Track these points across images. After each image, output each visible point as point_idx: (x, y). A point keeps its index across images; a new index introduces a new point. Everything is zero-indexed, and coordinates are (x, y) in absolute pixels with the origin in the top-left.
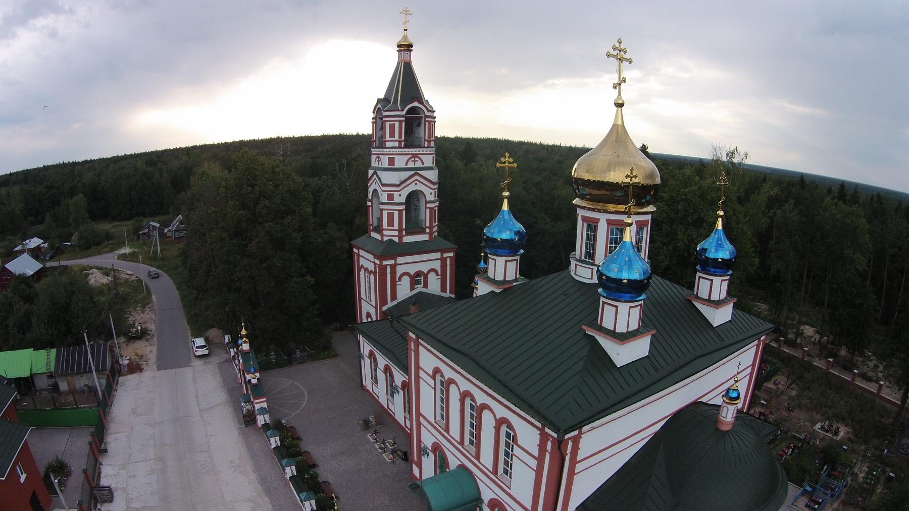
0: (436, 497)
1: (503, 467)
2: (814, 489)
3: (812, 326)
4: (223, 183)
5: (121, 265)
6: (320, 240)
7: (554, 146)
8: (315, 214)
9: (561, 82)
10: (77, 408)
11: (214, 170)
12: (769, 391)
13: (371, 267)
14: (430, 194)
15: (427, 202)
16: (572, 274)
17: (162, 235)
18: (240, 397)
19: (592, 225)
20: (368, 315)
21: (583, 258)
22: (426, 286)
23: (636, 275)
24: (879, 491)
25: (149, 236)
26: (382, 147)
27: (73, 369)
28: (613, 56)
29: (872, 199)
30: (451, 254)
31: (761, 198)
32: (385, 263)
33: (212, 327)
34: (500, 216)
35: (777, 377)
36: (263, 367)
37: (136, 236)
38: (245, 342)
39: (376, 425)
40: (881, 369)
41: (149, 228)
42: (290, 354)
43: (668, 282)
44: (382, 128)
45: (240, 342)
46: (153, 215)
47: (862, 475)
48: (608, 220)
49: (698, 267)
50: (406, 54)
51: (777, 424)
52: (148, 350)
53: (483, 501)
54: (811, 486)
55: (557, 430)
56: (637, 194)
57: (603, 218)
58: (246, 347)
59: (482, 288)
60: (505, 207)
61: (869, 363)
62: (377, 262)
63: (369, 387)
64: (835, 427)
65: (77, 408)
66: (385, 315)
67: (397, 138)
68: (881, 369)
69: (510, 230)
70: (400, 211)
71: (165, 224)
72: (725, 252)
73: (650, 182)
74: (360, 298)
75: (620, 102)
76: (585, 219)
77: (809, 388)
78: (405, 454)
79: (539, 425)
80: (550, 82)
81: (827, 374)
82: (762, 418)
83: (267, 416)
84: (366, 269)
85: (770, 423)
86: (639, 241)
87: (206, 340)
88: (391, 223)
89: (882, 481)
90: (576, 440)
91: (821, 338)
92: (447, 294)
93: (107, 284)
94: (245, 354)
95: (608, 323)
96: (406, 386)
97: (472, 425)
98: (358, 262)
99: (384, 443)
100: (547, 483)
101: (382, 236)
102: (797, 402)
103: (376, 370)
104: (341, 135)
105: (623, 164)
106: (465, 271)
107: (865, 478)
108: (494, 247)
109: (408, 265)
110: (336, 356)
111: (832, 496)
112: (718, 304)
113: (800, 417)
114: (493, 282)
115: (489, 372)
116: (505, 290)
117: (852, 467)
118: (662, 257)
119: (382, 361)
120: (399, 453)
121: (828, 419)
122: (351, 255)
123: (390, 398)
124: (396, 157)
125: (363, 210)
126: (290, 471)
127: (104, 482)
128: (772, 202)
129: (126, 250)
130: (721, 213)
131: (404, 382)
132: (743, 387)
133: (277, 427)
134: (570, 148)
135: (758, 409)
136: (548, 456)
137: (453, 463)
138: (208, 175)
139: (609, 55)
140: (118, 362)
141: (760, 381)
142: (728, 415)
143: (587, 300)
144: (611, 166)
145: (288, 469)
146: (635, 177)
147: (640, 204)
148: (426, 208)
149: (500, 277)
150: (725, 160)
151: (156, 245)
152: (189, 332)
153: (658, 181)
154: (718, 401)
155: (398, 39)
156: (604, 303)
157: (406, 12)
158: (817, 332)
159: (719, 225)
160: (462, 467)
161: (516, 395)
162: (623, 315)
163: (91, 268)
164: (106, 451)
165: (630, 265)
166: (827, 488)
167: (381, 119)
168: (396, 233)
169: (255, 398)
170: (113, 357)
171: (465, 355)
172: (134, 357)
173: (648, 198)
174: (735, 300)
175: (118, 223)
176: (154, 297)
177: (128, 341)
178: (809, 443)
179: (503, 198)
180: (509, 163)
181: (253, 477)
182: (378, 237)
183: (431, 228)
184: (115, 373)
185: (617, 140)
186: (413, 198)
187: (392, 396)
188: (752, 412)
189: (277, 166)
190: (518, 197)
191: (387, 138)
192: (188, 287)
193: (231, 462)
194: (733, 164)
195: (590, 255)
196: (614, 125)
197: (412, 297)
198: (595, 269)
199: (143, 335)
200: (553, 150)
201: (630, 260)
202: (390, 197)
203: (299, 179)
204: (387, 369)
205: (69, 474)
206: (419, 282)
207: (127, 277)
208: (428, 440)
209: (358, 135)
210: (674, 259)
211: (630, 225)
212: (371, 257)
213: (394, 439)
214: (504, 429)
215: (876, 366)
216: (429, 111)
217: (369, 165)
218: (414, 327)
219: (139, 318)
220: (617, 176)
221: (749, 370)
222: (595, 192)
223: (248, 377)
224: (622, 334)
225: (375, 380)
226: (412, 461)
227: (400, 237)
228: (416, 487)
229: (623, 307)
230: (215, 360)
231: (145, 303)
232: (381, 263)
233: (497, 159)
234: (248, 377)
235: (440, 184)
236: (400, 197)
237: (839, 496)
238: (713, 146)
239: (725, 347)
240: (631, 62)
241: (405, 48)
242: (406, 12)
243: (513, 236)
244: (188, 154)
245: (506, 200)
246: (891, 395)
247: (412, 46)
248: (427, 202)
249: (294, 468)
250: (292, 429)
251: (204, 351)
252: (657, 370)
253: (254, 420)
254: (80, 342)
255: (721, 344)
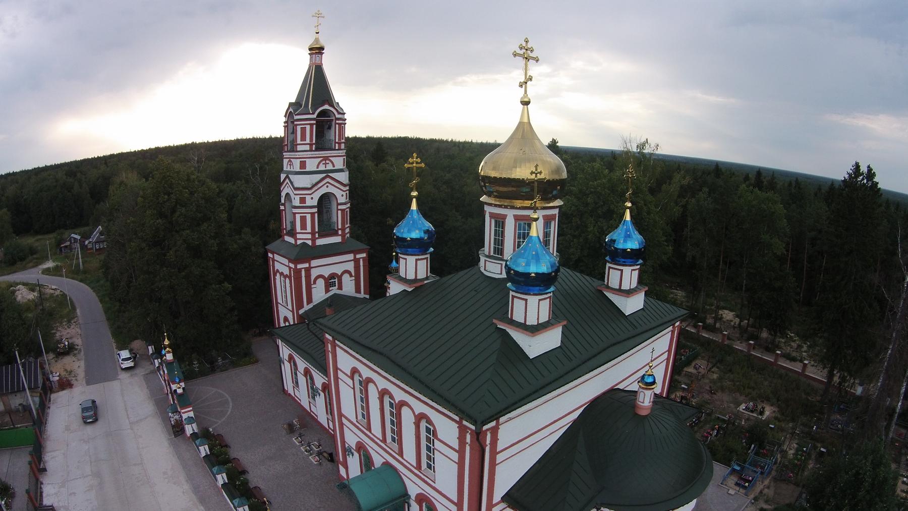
0: (365, 496)
1: (425, 463)
2: (743, 468)
3: (731, 311)
4: (141, 193)
5: (45, 280)
6: (235, 246)
7: (465, 143)
8: (230, 220)
9: (470, 79)
10: (14, 428)
11: (131, 178)
12: (689, 375)
13: (286, 271)
14: (341, 196)
15: (338, 204)
16: (482, 269)
17: (83, 247)
18: (167, 407)
19: (500, 222)
20: (286, 319)
21: (492, 254)
22: (340, 288)
23: (544, 268)
24: (810, 466)
25: (71, 249)
26: (293, 151)
27: (13, 386)
28: (520, 55)
29: (790, 184)
30: (364, 255)
31: (673, 188)
32: (299, 266)
33: (136, 338)
34: (409, 216)
35: (697, 362)
36: (188, 377)
37: (59, 249)
38: (169, 352)
39: (301, 428)
40: (805, 348)
41: (70, 241)
42: (212, 362)
43: (578, 274)
44: (294, 132)
45: (163, 352)
46: (74, 226)
47: (792, 452)
48: (515, 216)
49: (607, 258)
50: (318, 57)
51: (699, 408)
52: (76, 365)
53: (409, 497)
54: (739, 465)
55: (474, 422)
56: (544, 190)
58: (169, 357)
59: (395, 288)
60: (414, 206)
61: (793, 344)
62: (292, 266)
63: (291, 391)
64: (760, 407)
65: (14, 428)
66: (301, 318)
67: (308, 141)
68: (805, 348)
69: (420, 229)
70: (312, 214)
71: (86, 236)
72: (634, 243)
73: (557, 177)
74: (277, 303)
75: (526, 100)
76: (492, 215)
77: (730, 371)
78: (331, 455)
79: (457, 418)
80: (460, 79)
81: (749, 356)
82: (684, 402)
83: (194, 425)
84: (282, 274)
85: (692, 406)
86: (547, 235)
87: (131, 351)
88: (303, 226)
89: (813, 457)
90: (495, 431)
91: (741, 321)
92: (362, 295)
93: (33, 300)
94: (169, 364)
95: (518, 317)
96: (326, 387)
97: (392, 422)
99: (309, 446)
100: (469, 478)
101: (296, 240)
102: (719, 384)
103: (296, 374)
104: (254, 139)
105: (529, 160)
106: (378, 271)
107: (796, 454)
108: (405, 247)
109: (322, 267)
110: (257, 361)
111: (762, 473)
112: (629, 293)
113: (723, 399)
114: (404, 281)
115: (404, 369)
116: (417, 288)
117: (780, 445)
118: (572, 250)
119: (302, 364)
120: (325, 455)
121: (752, 399)
122: (266, 259)
123: (312, 401)
125: (276, 214)
126: (222, 479)
127: (47, 501)
128: (684, 191)
129: (50, 264)
130: (629, 204)
131: (324, 383)
132: (660, 373)
133: (204, 435)
134: (482, 144)
135: (679, 394)
136: (468, 448)
137: (378, 461)
138: (126, 185)
139: (515, 55)
140: (48, 379)
141: (677, 368)
142: (646, 400)
143: (497, 295)
144: (516, 163)
145: (219, 477)
146: (540, 173)
147: (546, 199)
148: (338, 210)
149: (411, 276)
150: (635, 150)
151: (78, 258)
152: (114, 345)
153: (564, 175)
154: (635, 387)
155: (310, 42)
156: (513, 297)
157: (319, 15)
158: (737, 316)
159: (628, 216)
160: (386, 464)
161: (433, 391)
162: (533, 308)
163: (17, 284)
164: (45, 470)
165: (537, 259)
166: (756, 466)
167: (293, 122)
168: (309, 236)
169: (182, 408)
170: (44, 374)
171: (381, 354)
172: (63, 374)
173: (555, 192)
174: (647, 289)
175: (40, 237)
176: (78, 311)
177: (57, 357)
178: (734, 424)
179: (411, 198)
180: (417, 163)
181: (186, 486)
182: (291, 240)
183: (343, 229)
184: (47, 390)
185: (523, 137)
186: (325, 200)
187: (314, 398)
188: (673, 396)
189: (192, 173)
190: (420, 194)
191: (299, 141)
192: (111, 299)
193: (165, 473)
194: (643, 155)
195: (499, 250)
196: (520, 123)
197: (327, 299)
198: (504, 263)
199: (70, 350)
200: (464, 147)
201: (537, 254)
202: (303, 200)
203: (214, 186)
204: (307, 372)
205: (12, 496)
206: (333, 284)
207: (52, 291)
208: (351, 439)
209: (271, 138)
210: (584, 251)
211: (536, 220)
212: (286, 261)
213: (319, 441)
214: (423, 424)
215: (799, 347)
216: (339, 113)
217: (281, 170)
218: (329, 328)
219: (67, 333)
220: (523, 173)
221: (665, 356)
222: (502, 189)
223: (174, 387)
224: (532, 326)
225: (296, 384)
226: (338, 462)
227: (313, 240)
228: (344, 486)
229: (533, 300)
230: (140, 372)
231: (70, 317)
232: (296, 266)
233: (406, 161)
234: (174, 387)
235: (350, 185)
236: (312, 200)
237: (769, 473)
238: (623, 138)
239: (639, 334)
240: (537, 61)
241: (317, 51)
242: (319, 15)
243: (422, 235)
244: (106, 163)
245: (414, 200)
246: (816, 373)
247: (322, 48)
248: (338, 204)
249: (224, 475)
250: (220, 436)
251: (130, 364)
252: (570, 360)
253: (183, 430)
254: (12, 360)
255: (635, 332)
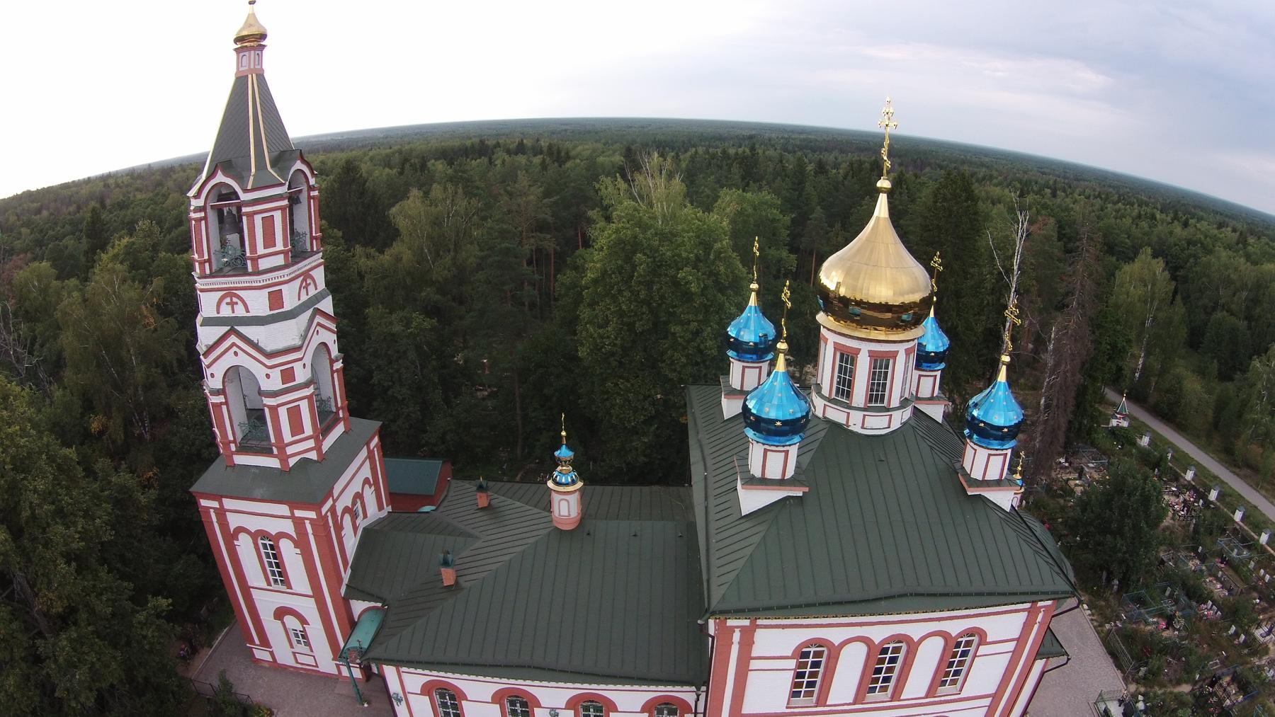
11: (660, 189)
14: (331, 339)
19: (847, 359)
21: (833, 396)
57: (865, 348)
67: (280, 246)
79: (1073, 580)
84: (258, 535)
95: (756, 471)
98: (224, 524)
124: (284, 288)
174: (943, 366)
182: (273, 463)
202: (288, 375)
212: (284, 510)
232: (319, 514)
247: (263, 36)
